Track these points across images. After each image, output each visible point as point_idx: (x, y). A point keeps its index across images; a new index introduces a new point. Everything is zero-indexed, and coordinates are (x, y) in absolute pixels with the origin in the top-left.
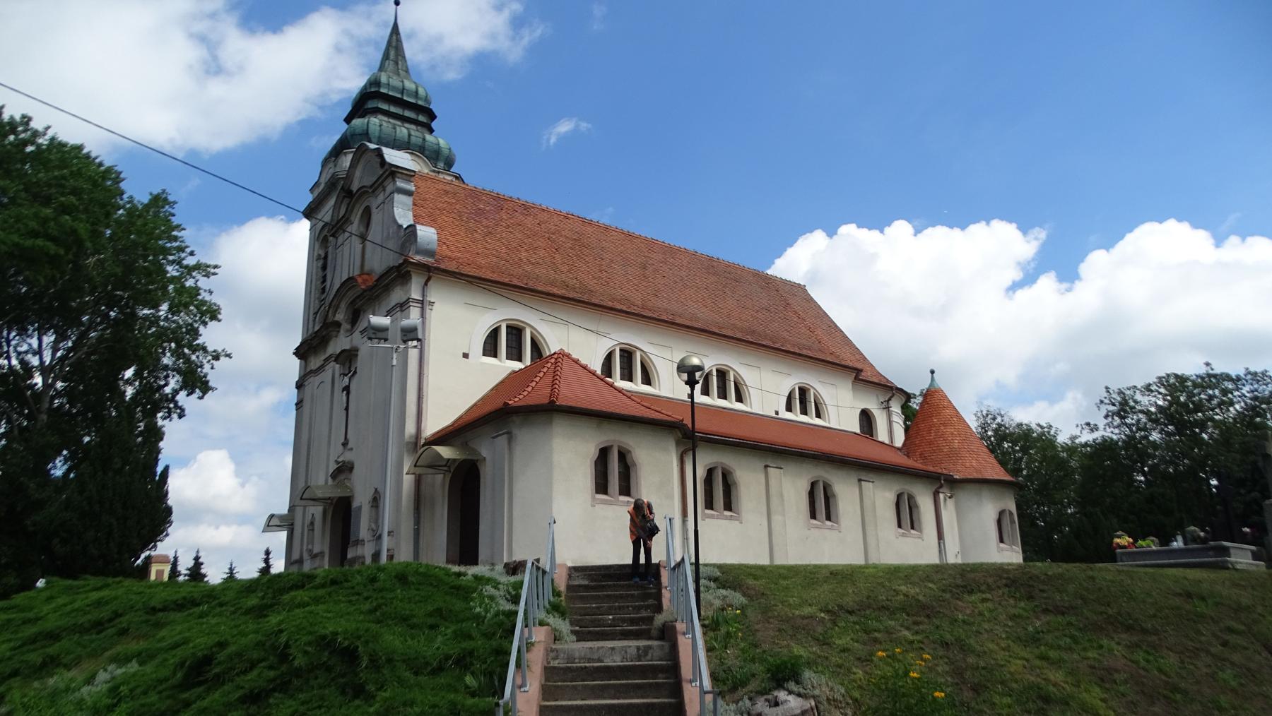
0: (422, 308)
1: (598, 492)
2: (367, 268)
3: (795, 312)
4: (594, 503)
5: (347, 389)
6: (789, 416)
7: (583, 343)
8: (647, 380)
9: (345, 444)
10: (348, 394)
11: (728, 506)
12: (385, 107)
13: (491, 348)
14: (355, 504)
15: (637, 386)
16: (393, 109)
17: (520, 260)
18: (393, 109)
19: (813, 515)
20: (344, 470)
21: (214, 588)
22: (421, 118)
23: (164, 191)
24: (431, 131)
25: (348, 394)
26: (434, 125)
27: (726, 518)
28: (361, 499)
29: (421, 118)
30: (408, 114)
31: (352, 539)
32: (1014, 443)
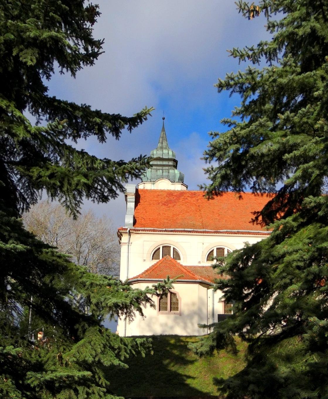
29: (171, 163)
30: (165, 163)
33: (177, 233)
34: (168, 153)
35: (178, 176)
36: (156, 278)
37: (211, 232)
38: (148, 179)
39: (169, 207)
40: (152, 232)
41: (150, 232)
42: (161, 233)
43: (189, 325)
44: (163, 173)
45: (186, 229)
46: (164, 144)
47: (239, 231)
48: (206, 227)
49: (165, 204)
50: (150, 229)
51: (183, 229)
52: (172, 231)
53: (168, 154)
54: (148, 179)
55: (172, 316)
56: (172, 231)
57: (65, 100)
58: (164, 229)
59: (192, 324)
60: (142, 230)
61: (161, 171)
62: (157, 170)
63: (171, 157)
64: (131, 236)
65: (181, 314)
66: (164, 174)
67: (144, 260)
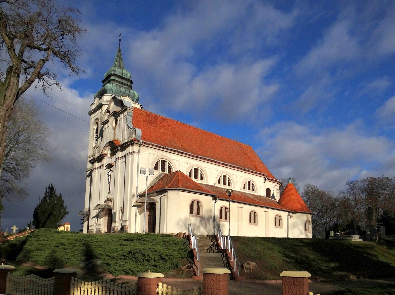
1: (225, 219)
3: (248, 157)
4: (275, 228)
7: (182, 164)
8: (202, 179)
9: (109, 193)
12: (117, 79)
13: (156, 168)
14: (114, 211)
15: (251, 192)
17: (165, 139)
19: (250, 221)
20: (109, 200)
22: (129, 83)
23: (275, 228)
26: (132, 85)
28: (117, 210)
29: (129, 83)
30: (124, 82)
31: (113, 221)
32: (178, 291)
35: (136, 97)
36: (174, 187)
37: (192, 156)
38: (113, 92)
41: (155, 147)
42: (163, 149)
43: (208, 225)
44: (125, 90)
45: (172, 149)
46: (121, 64)
47: (209, 159)
48: (186, 151)
49: (150, 122)
50: (155, 144)
53: (127, 74)
54: (113, 92)
57: (7, 68)
58: (165, 147)
60: (150, 144)
61: (124, 89)
62: (120, 87)
63: (128, 78)
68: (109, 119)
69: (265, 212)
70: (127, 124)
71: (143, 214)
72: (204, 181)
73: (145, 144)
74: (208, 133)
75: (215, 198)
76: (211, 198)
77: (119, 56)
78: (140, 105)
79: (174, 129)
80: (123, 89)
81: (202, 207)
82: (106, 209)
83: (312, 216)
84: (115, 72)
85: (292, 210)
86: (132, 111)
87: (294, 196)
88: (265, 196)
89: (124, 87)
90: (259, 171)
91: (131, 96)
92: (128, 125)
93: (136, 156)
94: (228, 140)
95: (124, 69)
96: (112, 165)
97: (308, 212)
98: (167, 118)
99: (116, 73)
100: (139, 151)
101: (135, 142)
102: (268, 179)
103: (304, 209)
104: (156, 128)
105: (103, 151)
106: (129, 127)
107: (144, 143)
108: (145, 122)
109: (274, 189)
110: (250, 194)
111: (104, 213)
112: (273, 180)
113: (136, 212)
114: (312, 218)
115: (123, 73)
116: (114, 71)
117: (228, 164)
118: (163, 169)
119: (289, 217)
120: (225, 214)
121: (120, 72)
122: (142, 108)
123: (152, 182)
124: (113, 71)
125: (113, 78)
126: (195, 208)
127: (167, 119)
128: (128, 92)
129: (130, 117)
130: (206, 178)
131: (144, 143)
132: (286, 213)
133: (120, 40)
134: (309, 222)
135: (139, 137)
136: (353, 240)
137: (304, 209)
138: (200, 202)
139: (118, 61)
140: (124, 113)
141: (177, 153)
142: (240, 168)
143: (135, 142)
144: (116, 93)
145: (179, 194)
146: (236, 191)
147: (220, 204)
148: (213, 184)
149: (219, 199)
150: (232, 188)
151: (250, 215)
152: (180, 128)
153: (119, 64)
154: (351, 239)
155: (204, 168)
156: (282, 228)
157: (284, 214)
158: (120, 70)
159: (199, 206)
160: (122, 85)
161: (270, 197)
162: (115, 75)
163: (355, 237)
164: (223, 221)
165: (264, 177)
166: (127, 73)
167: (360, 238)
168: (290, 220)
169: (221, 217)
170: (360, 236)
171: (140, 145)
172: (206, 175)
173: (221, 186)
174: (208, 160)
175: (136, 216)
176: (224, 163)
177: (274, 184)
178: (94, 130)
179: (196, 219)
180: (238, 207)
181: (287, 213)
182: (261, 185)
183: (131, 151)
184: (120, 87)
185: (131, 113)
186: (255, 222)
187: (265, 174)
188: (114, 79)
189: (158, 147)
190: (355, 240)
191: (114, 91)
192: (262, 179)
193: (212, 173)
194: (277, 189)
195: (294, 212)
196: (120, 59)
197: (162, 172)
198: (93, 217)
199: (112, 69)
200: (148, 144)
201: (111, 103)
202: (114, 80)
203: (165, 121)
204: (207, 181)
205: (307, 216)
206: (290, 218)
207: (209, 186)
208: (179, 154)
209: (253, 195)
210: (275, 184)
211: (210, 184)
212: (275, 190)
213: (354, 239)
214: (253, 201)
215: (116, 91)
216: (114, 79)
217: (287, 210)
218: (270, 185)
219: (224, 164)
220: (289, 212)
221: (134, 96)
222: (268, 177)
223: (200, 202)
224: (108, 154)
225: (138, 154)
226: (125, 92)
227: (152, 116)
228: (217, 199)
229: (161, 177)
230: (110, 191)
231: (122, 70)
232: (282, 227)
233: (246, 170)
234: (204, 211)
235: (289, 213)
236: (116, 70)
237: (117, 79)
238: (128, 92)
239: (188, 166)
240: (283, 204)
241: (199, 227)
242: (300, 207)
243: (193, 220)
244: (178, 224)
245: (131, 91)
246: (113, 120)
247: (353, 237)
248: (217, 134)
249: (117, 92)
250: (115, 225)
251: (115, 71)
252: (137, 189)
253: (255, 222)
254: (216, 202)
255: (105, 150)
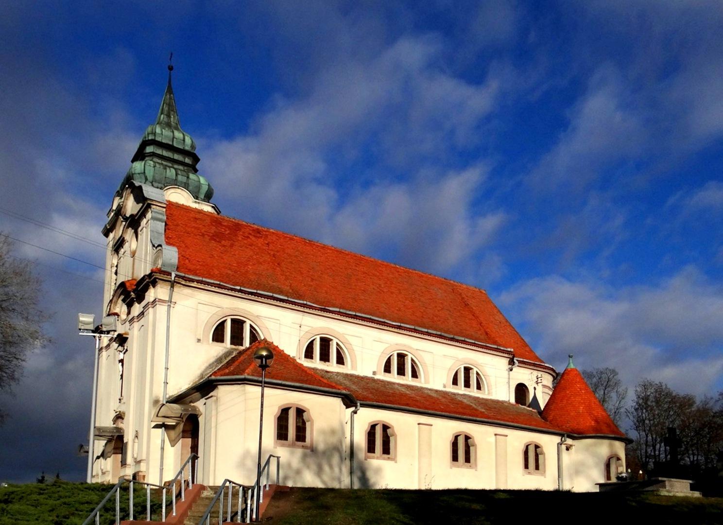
0: (169, 306)
2: (134, 278)
5: (122, 361)
6: (387, 378)
7: (286, 329)
10: (123, 365)
11: (468, 460)
12: (159, 151)
13: (218, 336)
15: (473, 392)
16: (165, 153)
17: (247, 272)
18: (165, 153)
19: (526, 466)
21: (356, 490)
22: (188, 160)
24: (196, 171)
25: (123, 365)
26: (198, 166)
27: (384, 459)
29: (188, 160)
30: (176, 157)
33: (260, 299)
34: (184, 139)
35: (205, 189)
37: (315, 308)
38: (146, 179)
39: (224, 246)
40: (217, 290)
41: (213, 289)
43: (326, 468)
46: (172, 119)
49: (217, 237)
51: (271, 294)
52: (252, 294)
53: (184, 140)
54: (146, 179)
55: (299, 452)
56: (252, 294)
58: (238, 288)
59: (331, 467)
60: (198, 282)
61: (173, 171)
63: (187, 148)
64: (175, 289)
65: (313, 450)
66: (180, 178)
67: (199, 340)
68: (124, 236)
69: (496, 435)
70: (151, 240)
71: (179, 444)
72: (347, 366)
73: (186, 280)
74: (372, 261)
75: (349, 401)
76: (337, 402)
77: (168, 101)
78: (213, 207)
79: (278, 251)
80: (170, 173)
81: (312, 425)
82: (115, 438)
83: (626, 444)
84: (155, 136)
85: (573, 431)
86: (164, 210)
87: (578, 399)
88: (513, 400)
89: (175, 169)
90: (495, 343)
91: (190, 188)
92: (152, 243)
93: (162, 309)
94: (422, 276)
95: (177, 129)
96: (124, 336)
97: (613, 436)
98: (266, 229)
99: (157, 139)
100: (171, 296)
101: (158, 275)
102: (520, 362)
103: (604, 428)
104: (229, 249)
105: (112, 308)
106: (154, 246)
107: (183, 278)
108: (203, 235)
109: (536, 386)
110: (470, 397)
111: (112, 447)
112: (534, 365)
113: (163, 441)
114: (626, 450)
115: (174, 138)
116: (152, 133)
117: (408, 326)
118: (237, 338)
119: (564, 447)
120: (381, 440)
121: (166, 137)
122: (218, 214)
123: (207, 368)
124: (150, 135)
125: (149, 149)
126: (291, 426)
127: (265, 231)
128: (184, 179)
129: (158, 222)
130: (351, 359)
131: (183, 278)
132: (557, 439)
133: (171, 68)
134: (619, 459)
135: (171, 265)
136: (664, 493)
137: (604, 428)
138: (470, 438)
139: (165, 112)
140: (147, 216)
141: (272, 302)
142: (441, 337)
143: (158, 275)
144: (155, 182)
145: (245, 390)
146: (430, 390)
147: (367, 416)
148: (370, 375)
149: (363, 405)
150: (421, 382)
151: (455, 445)
152: (297, 251)
153: (166, 120)
154: (658, 491)
155: (347, 337)
156: (544, 474)
157: (549, 443)
158: (167, 132)
159: (303, 420)
160: (170, 165)
161: (527, 404)
162: (154, 142)
163: (672, 486)
164: (378, 458)
165: (506, 355)
166: (184, 138)
167: (693, 488)
168: (565, 456)
169: (371, 448)
170: (691, 482)
171: (173, 284)
172: (351, 351)
173: (393, 377)
174: (355, 317)
175: (162, 449)
176: (399, 324)
177: (535, 373)
178: (112, 267)
179: (292, 453)
180: (419, 424)
181: (557, 439)
182: (499, 379)
183: (152, 299)
184: (165, 167)
185: (161, 214)
186: (537, 468)
187: (509, 350)
188: (152, 151)
189: (220, 286)
190: (671, 494)
191: (150, 178)
192: (501, 362)
193: (367, 349)
194: (544, 386)
195: (575, 435)
196: (169, 109)
197: (233, 347)
198: (98, 458)
199: (149, 129)
200: (193, 281)
201: (127, 199)
202: (153, 155)
203: (258, 235)
204: (354, 367)
205: (611, 446)
206: (567, 449)
207: (358, 377)
208: (278, 303)
209: (476, 399)
210: (539, 374)
211: (362, 374)
212: (539, 389)
213: (668, 491)
214: (468, 411)
215: (154, 176)
216: (153, 152)
217: (557, 431)
218: (524, 375)
219: (399, 327)
220: (562, 435)
221: (199, 186)
222: (519, 354)
223: (470, 438)
224: (120, 312)
225: (167, 304)
226: (176, 180)
227: (225, 224)
228: (359, 404)
229: (230, 358)
230: (121, 396)
231: (173, 132)
232: (545, 472)
233: (457, 341)
234: (316, 432)
235: (563, 439)
236: (158, 130)
237: (159, 151)
238: (184, 179)
239: (302, 333)
240: (551, 418)
241: (298, 472)
242: (593, 423)
243: (287, 455)
244: (242, 464)
245: (192, 176)
246: (132, 236)
247: (667, 483)
248: (395, 264)
249: (157, 179)
250: (125, 472)
251: (155, 134)
252: (165, 387)
253: (537, 468)
254: (358, 412)
255: (116, 305)
